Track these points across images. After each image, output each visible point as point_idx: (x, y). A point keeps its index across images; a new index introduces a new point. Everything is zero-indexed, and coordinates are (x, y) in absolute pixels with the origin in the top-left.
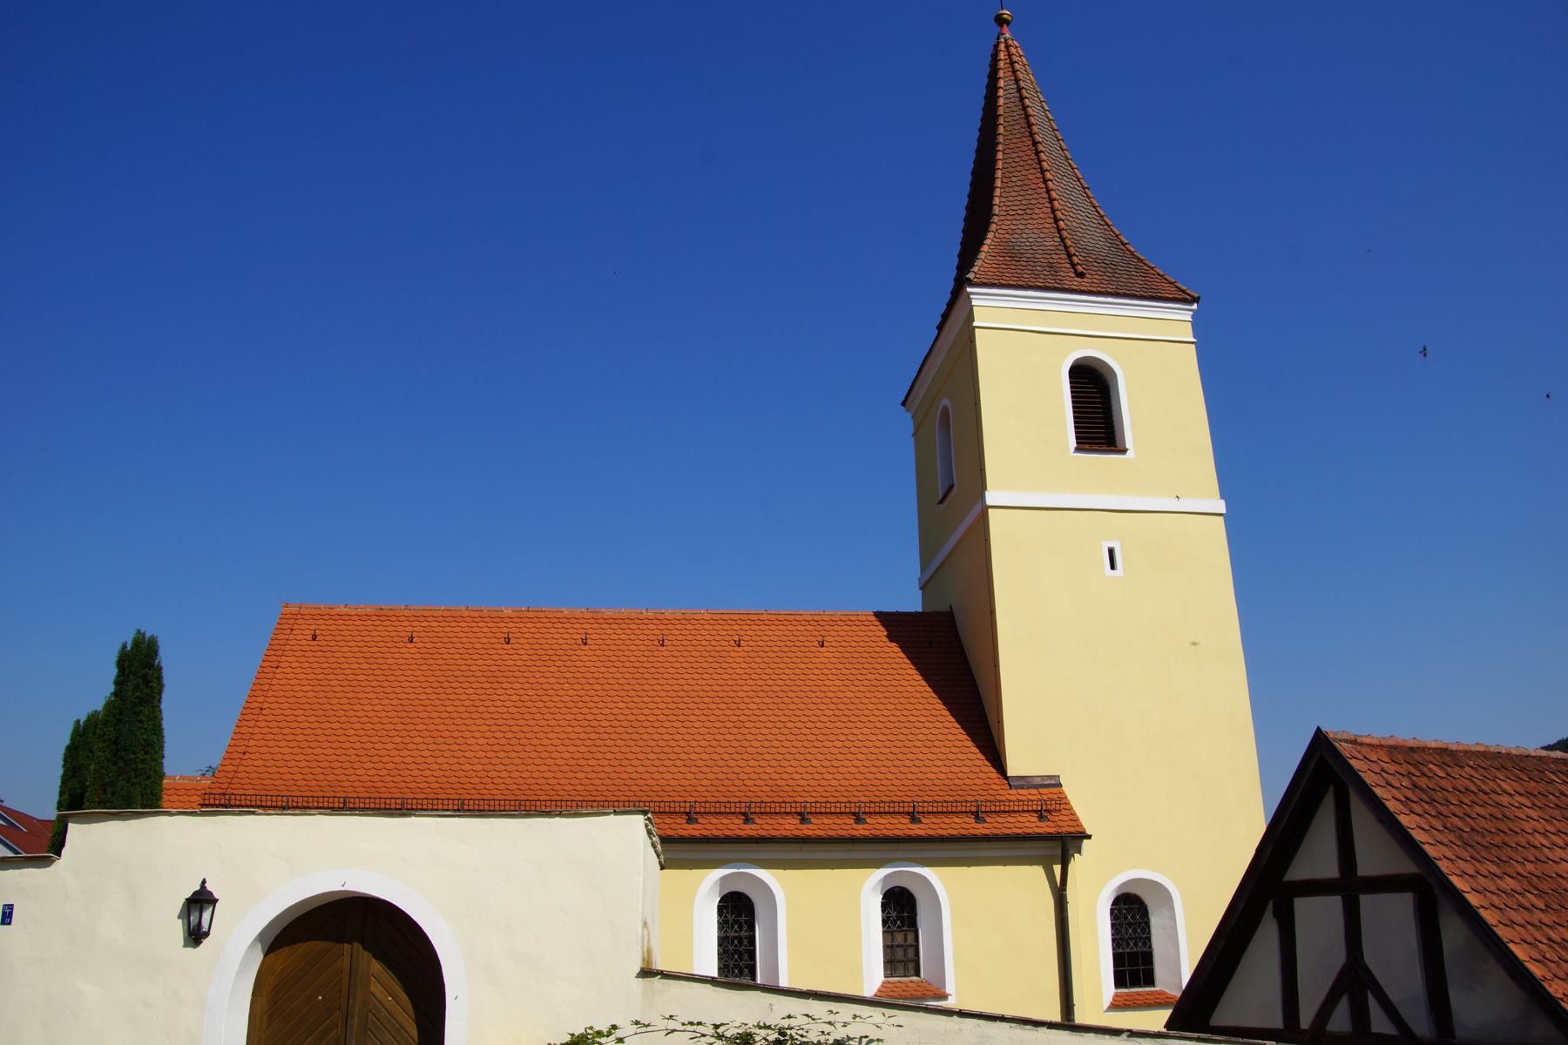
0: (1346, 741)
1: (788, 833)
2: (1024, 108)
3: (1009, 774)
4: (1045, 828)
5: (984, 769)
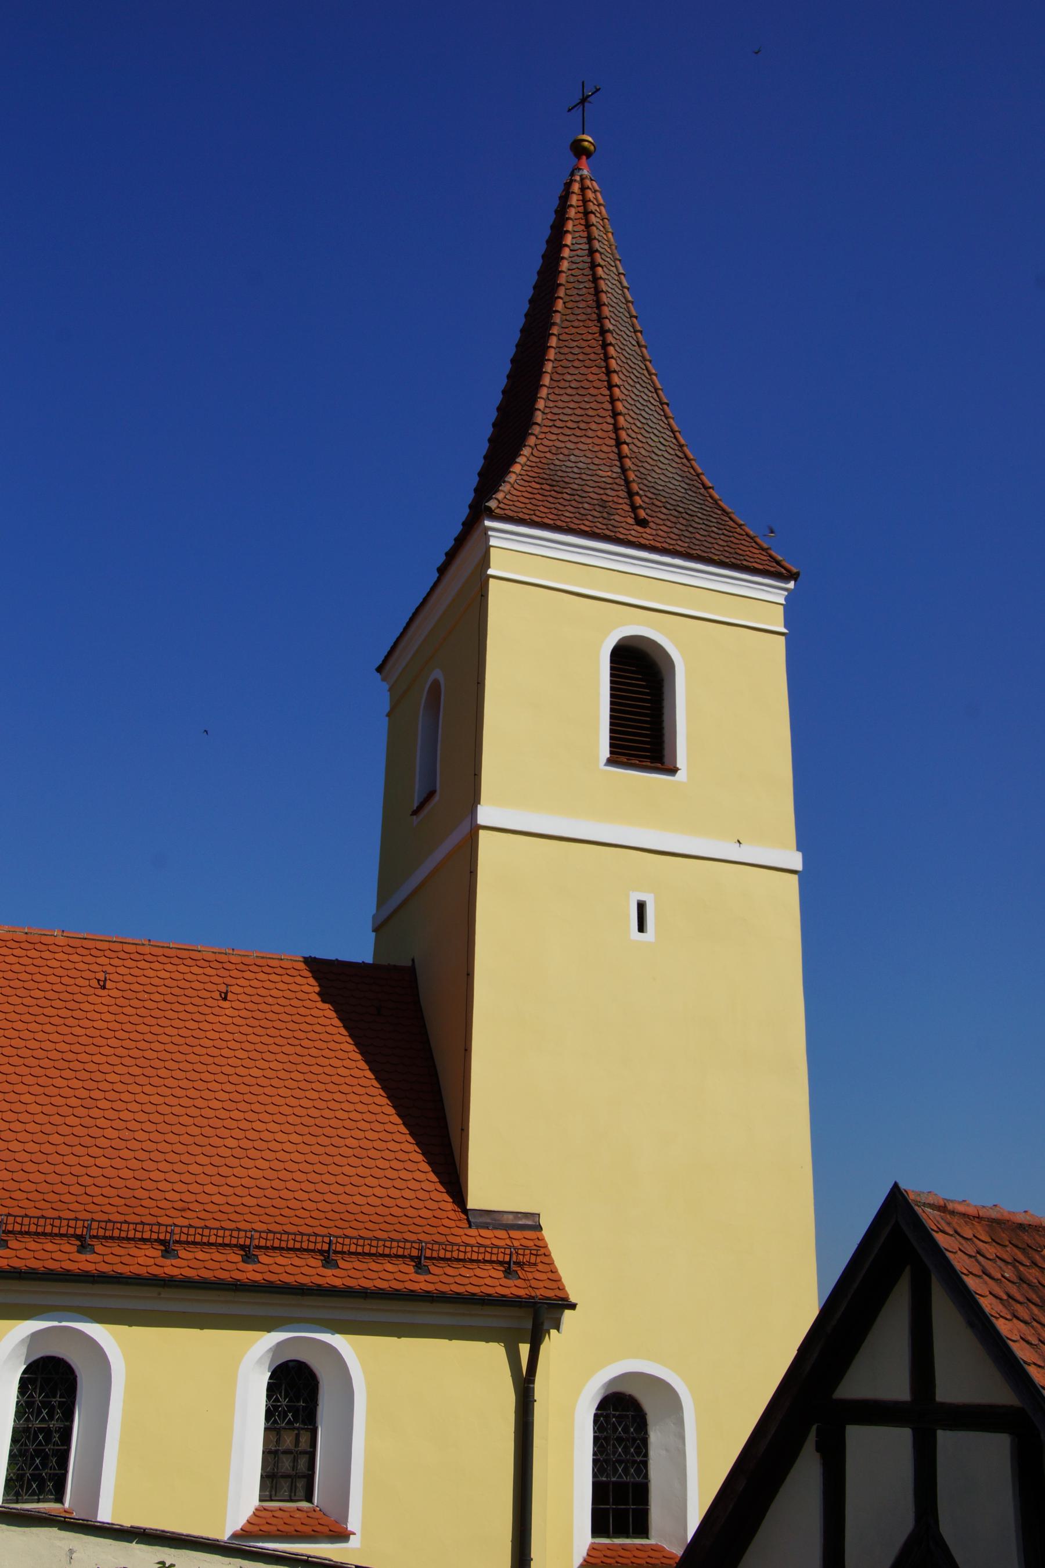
0: (931, 1206)
1: (142, 1271)
2: (595, 279)
3: (471, 1204)
4: (512, 1288)
5: (435, 1195)
